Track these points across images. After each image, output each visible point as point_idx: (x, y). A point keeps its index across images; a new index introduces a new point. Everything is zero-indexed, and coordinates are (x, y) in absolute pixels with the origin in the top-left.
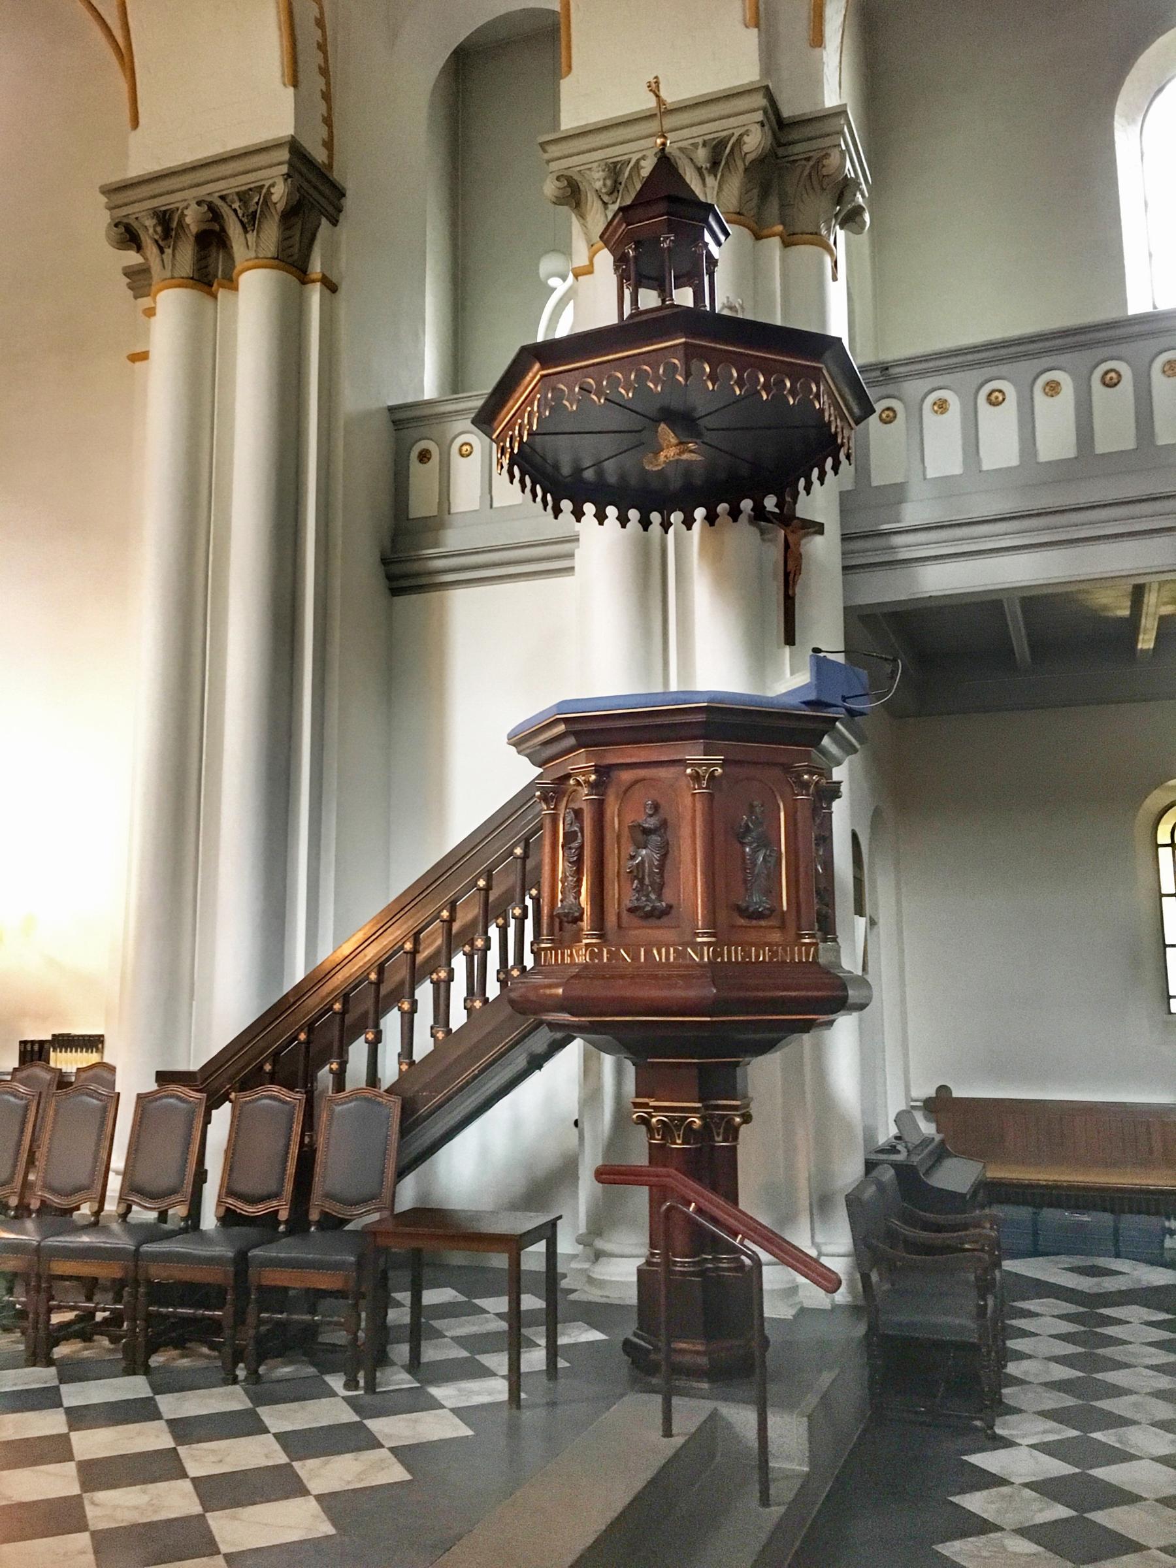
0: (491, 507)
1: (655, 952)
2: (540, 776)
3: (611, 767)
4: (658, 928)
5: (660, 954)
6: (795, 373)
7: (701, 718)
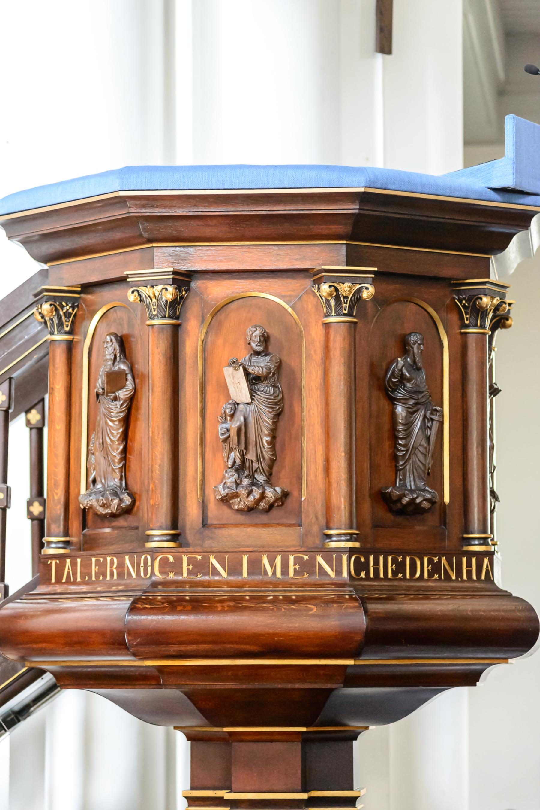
1: (265, 561)
2: (44, 274)
3: (190, 275)
4: (265, 525)
5: (272, 562)
7: (353, 208)
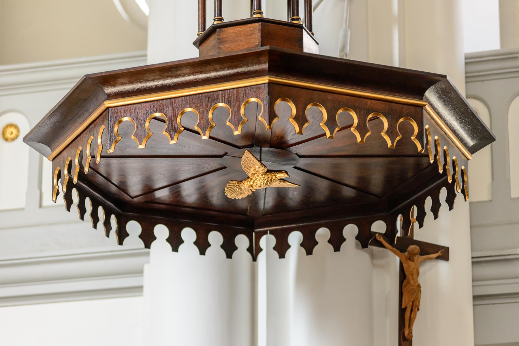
0: (41, 206)
6: (394, 112)
